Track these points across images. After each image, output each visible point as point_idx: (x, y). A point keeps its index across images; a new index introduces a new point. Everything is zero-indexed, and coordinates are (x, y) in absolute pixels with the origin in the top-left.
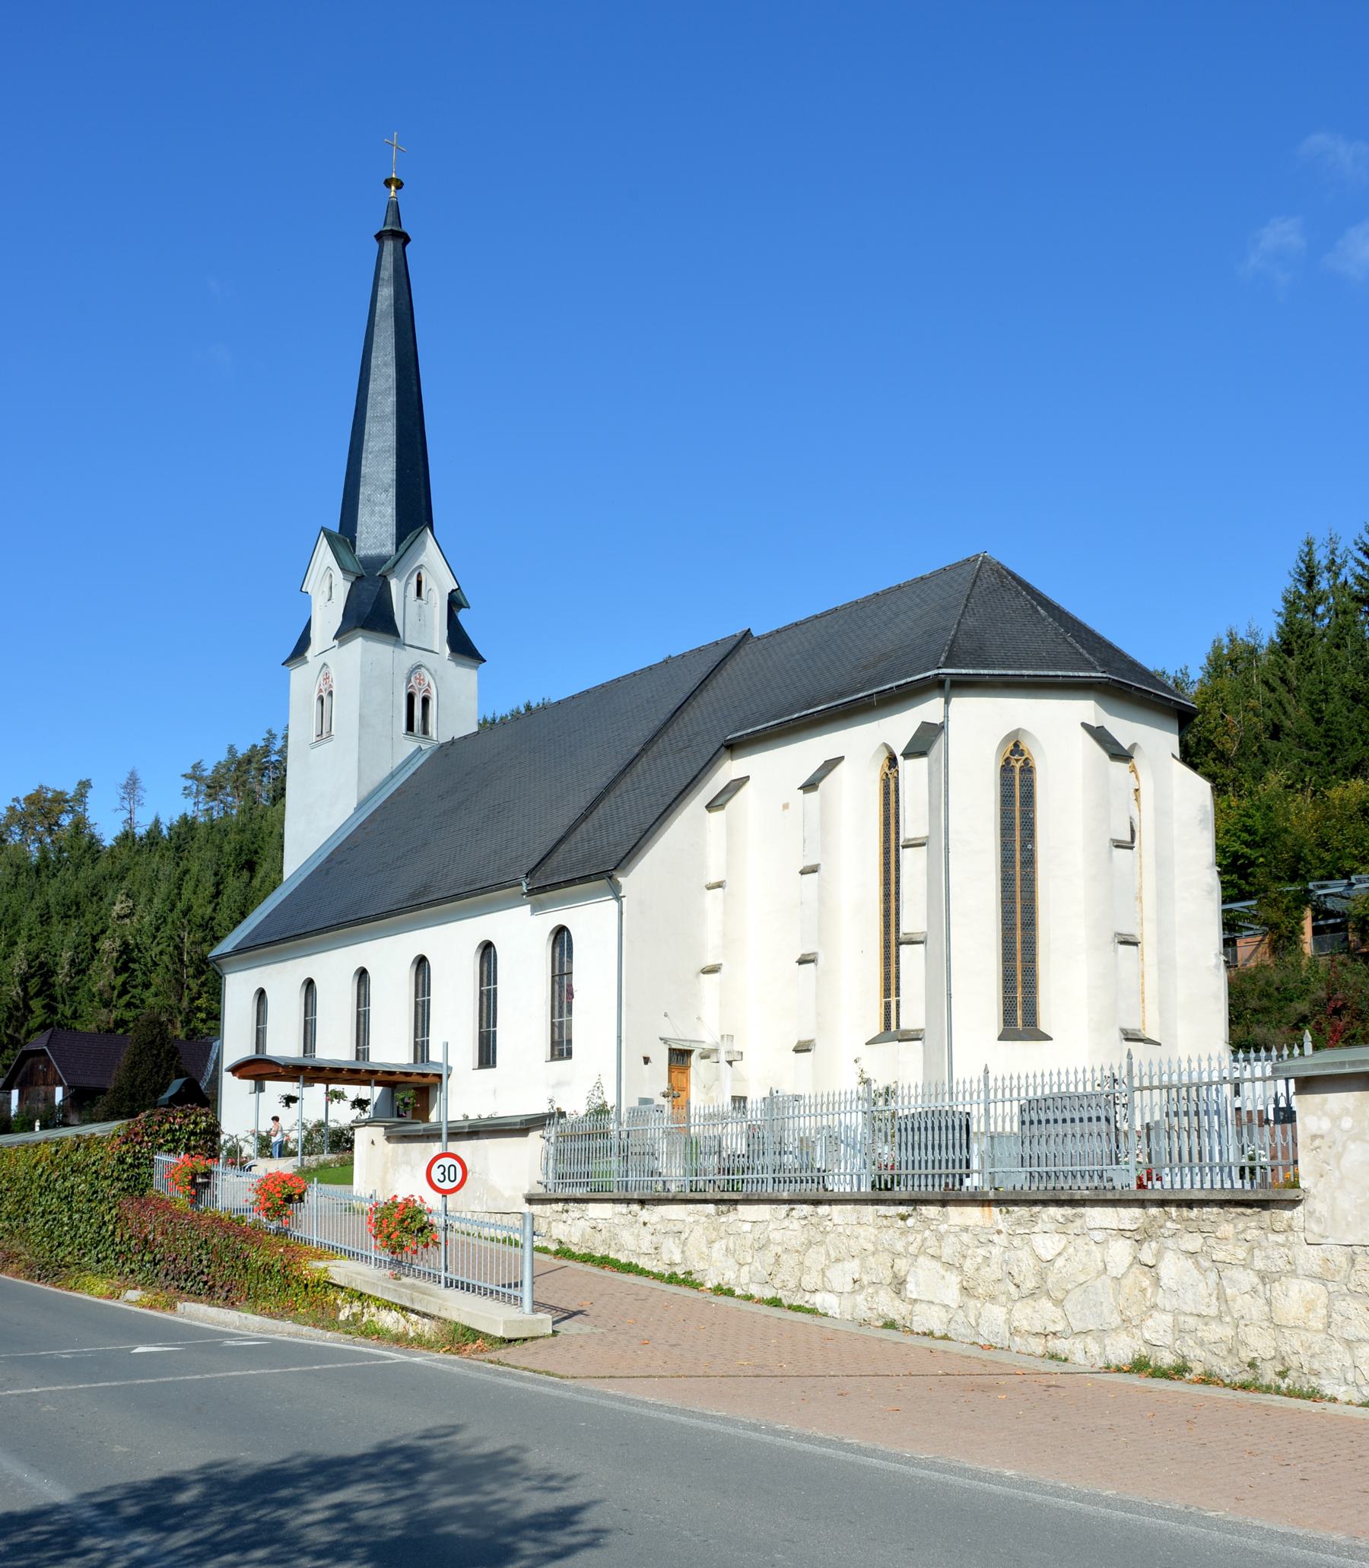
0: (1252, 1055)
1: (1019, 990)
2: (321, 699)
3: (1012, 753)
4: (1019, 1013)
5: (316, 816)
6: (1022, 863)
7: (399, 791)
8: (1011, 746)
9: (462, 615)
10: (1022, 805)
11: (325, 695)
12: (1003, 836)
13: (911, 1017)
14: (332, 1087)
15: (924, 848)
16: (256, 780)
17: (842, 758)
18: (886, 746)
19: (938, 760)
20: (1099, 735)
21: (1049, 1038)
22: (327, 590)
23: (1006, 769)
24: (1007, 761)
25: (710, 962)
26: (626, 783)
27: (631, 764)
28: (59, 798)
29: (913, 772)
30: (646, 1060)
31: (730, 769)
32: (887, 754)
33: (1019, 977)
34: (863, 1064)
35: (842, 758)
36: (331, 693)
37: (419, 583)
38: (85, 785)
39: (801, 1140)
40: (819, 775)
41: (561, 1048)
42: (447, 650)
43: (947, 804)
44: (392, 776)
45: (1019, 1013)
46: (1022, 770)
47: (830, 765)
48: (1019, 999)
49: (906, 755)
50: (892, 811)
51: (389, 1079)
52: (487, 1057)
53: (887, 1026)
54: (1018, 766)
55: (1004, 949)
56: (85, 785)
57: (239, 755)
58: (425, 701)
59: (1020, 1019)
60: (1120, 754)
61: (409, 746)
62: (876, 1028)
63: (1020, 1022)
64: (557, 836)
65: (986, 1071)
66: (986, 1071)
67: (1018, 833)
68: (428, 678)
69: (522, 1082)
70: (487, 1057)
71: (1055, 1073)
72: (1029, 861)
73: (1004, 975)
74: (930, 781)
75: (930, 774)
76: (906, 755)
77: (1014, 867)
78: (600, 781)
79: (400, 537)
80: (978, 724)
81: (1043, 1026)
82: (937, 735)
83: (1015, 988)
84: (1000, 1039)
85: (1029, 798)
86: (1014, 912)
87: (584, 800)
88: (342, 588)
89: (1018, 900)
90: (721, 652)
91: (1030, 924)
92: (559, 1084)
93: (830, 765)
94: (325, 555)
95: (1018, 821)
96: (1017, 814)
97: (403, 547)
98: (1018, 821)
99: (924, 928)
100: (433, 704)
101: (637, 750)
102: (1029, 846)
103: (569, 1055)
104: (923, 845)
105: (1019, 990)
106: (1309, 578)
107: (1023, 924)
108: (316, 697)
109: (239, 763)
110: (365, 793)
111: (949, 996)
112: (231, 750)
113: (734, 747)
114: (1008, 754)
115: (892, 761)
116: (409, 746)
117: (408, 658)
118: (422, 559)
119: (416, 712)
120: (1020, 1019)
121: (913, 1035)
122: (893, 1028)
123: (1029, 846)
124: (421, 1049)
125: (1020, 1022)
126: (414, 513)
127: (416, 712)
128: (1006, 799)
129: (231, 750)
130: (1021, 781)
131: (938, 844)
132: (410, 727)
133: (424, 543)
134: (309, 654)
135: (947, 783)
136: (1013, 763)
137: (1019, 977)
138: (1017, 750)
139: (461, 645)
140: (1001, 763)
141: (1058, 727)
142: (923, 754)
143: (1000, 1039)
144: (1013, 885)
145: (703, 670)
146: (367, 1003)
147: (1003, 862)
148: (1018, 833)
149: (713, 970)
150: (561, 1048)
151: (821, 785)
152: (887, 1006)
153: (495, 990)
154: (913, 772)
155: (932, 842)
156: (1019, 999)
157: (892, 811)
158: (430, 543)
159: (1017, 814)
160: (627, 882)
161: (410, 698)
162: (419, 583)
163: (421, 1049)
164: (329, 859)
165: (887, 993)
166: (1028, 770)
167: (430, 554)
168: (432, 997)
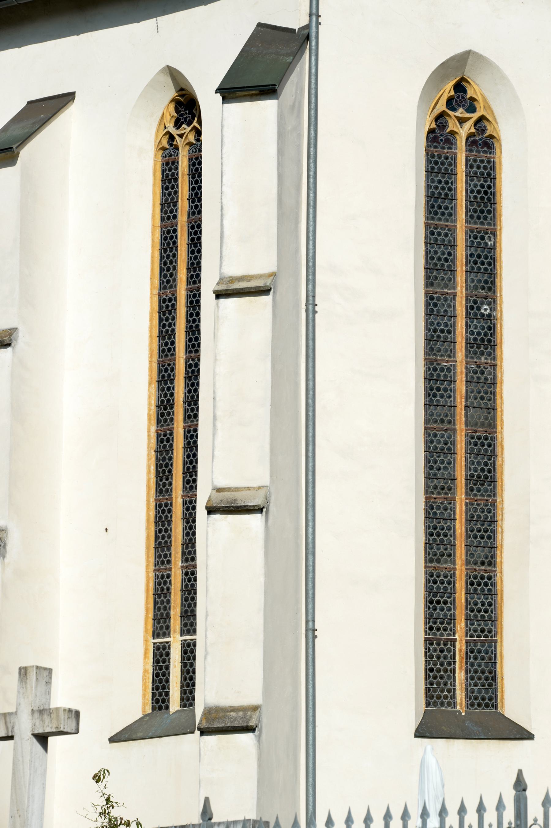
1: (461, 626)
3: (450, 103)
4: (460, 676)
6: (470, 345)
8: (448, 89)
10: (470, 217)
12: (429, 282)
13: (227, 673)
15: (267, 299)
17: (69, 97)
18: (173, 74)
19: (296, 107)
21: (529, 736)
23: (438, 137)
24: (440, 118)
29: (239, 134)
32: (172, 93)
33: (461, 597)
34: (111, 785)
35: (69, 97)
40: (18, 131)
43: (312, 205)
45: (460, 676)
46: (472, 142)
47: (43, 111)
48: (460, 646)
49: (229, 92)
50: (183, 219)
53: (160, 699)
54: (464, 132)
55: (429, 534)
62: (134, 703)
63: (460, 696)
65: (520, 785)
66: (520, 785)
67: (461, 278)
71: (397, 814)
72: (485, 340)
73: (429, 590)
74: (281, 152)
75: (281, 135)
76: (229, 92)
77: (452, 353)
81: (512, 707)
82: (297, 54)
83: (452, 619)
84: (420, 733)
86: (451, 451)
89: (460, 425)
91: (485, 478)
93: (43, 111)
95: (461, 253)
98: (461, 253)
99: (265, 480)
102: (485, 309)
104: (264, 291)
105: (461, 626)
107: (470, 478)
111: (311, 633)
114: (442, 107)
115: (186, 107)
121: (236, 720)
122: (175, 703)
123: (485, 309)
125: (460, 696)
128: (438, 201)
130: (469, 166)
135: (313, 159)
136: (453, 125)
137: (461, 597)
138: (461, 96)
140: (428, 123)
142: (268, 91)
143: (420, 733)
144: (450, 393)
147: (428, 340)
148: (461, 278)
151: (25, 153)
152: (161, 656)
154: (239, 134)
155: (282, 287)
156: (460, 646)
157: (183, 219)
165: (160, 624)
166: (484, 142)
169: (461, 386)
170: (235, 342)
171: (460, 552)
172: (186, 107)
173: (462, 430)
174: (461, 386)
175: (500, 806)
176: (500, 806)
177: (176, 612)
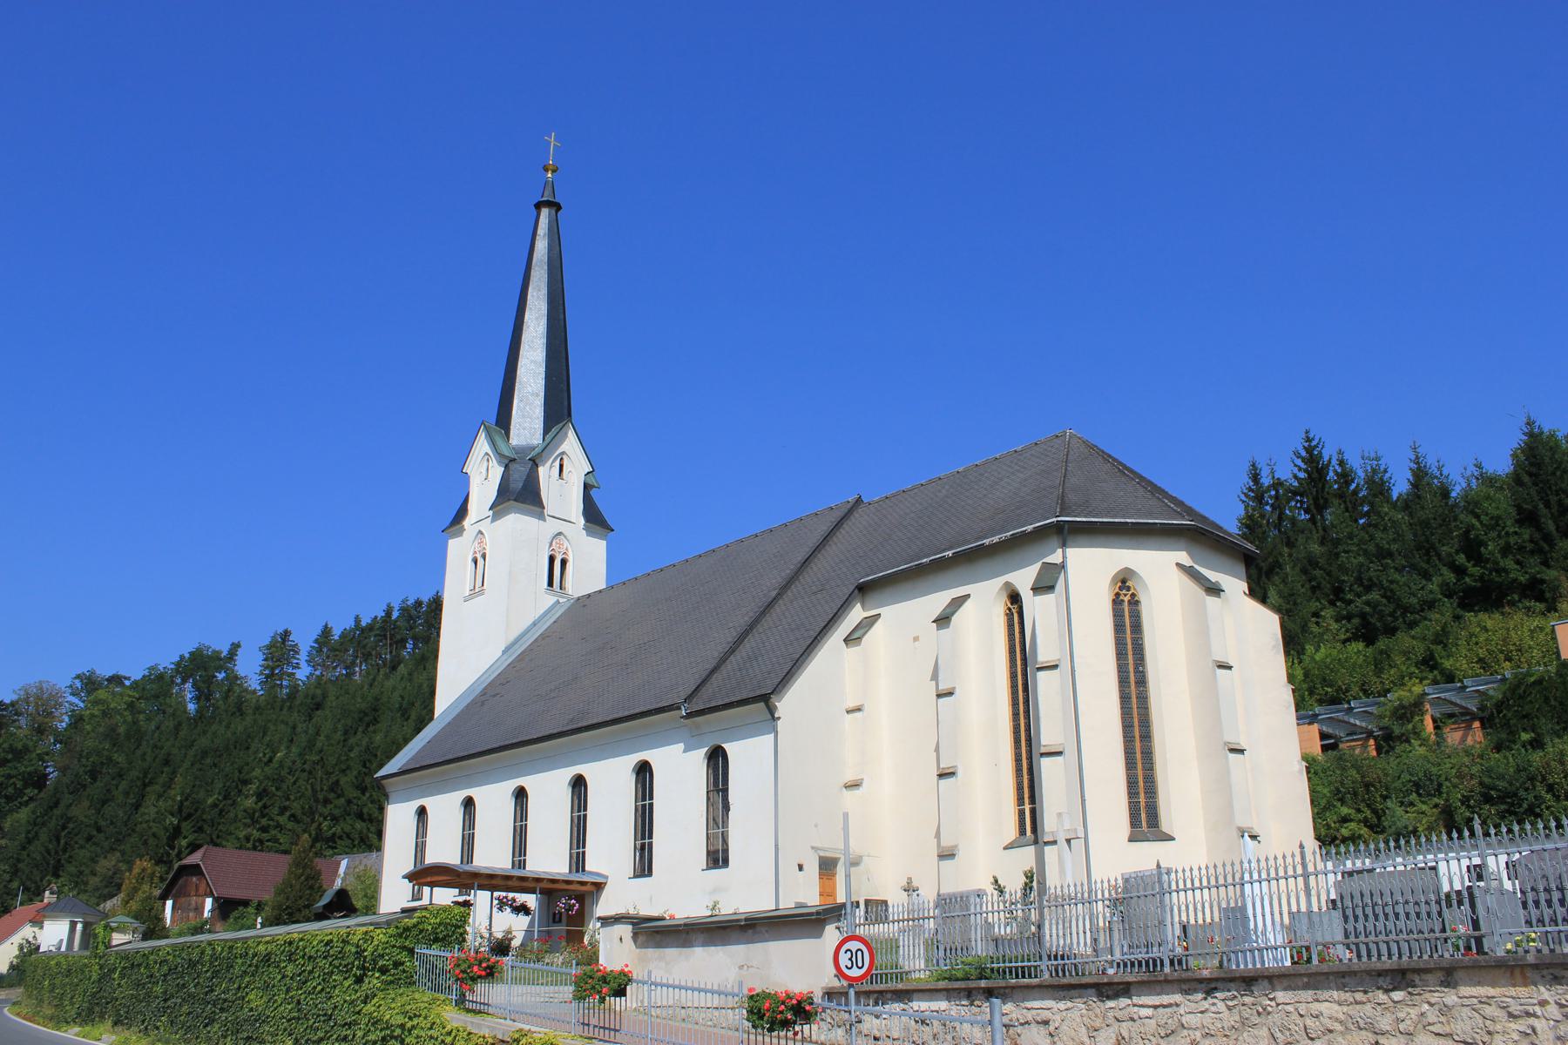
0: (1342, 849)
1: (1142, 795)
2: (475, 561)
5: (463, 665)
7: (543, 636)
9: (593, 492)
11: (479, 556)
14: (496, 894)
16: (416, 629)
20: (1190, 572)
22: (483, 476)
23: (1117, 602)
24: (1117, 595)
25: (850, 777)
26: (767, 621)
27: (770, 605)
28: (216, 656)
30: (801, 868)
31: (857, 613)
36: (484, 556)
37: (561, 466)
38: (235, 647)
39: (1184, 928)
41: (718, 858)
42: (582, 521)
44: (534, 624)
51: (549, 889)
52: (644, 867)
54: (1126, 599)
56: (235, 647)
57: (364, 624)
58: (564, 562)
59: (1145, 818)
60: (1214, 590)
61: (550, 600)
63: (1144, 824)
64: (710, 667)
65: (1301, 846)
66: (1301, 846)
67: (1130, 657)
68: (566, 544)
69: (680, 889)
70: (644, 867)
72: (1142, 681)
76: (1038, 589)
78: (742, 620)
79: (546, 431)
80: (1091, 567)
81: (1165, 826)
85: (1137, 627)
87: (731, 636)
88: (497, 471)
90: (838, 514)
91: (1147, 736)
92: (715, 891)
94: (482, 445)
95: (1130, 647)
96: (1129, 641)
97: (549, 437)
100: (569, 566)
101: (774, 593)
103: (726, 862)
105: (1142, 795)
106: (1255, 477)
108: (470, 558)
109: (363, 630)
110: (511, 639)
112: (357, 620)
113: (863, 590)
116: (550, 600)
117: (551, 526)
118: (564, 447)
119: (556, 568)
120: (1145, 818)
124: (578, 861)
125: (1144, 824)
126: (557, 411)
127: (556, 568)
128: (1119, 627)
129: (357, 620)
131: (1066, 665)
132: (550, 583)
133: (566, 435)
134: (467, 523)
139: (594, 517)
141: (1160, 570)
142: (1050, 588)
145: (824, 528)
146: (424, 835)
148: (1130, 657)
149: (854, 785)
150: (718, 858)
153: (651, 805)
156: (1143, 804)
158: (571, 434)
159: (1129, 641)
160: (785, 705)
161: (552, 559)
162: (561, 466)
163: (578, 861)
164: (484, 693)
166: (1134, 603)
167: (570, 443)
168: (655, 801)
169: (1134, 700)
170: (1047, 687)
171: (1140, 766)
172: (1015, 598)
173: (479, 1026)
174: (1134, 700)
175: (1293, 855)
176: (1293, 855)
177: (1026, 796)
